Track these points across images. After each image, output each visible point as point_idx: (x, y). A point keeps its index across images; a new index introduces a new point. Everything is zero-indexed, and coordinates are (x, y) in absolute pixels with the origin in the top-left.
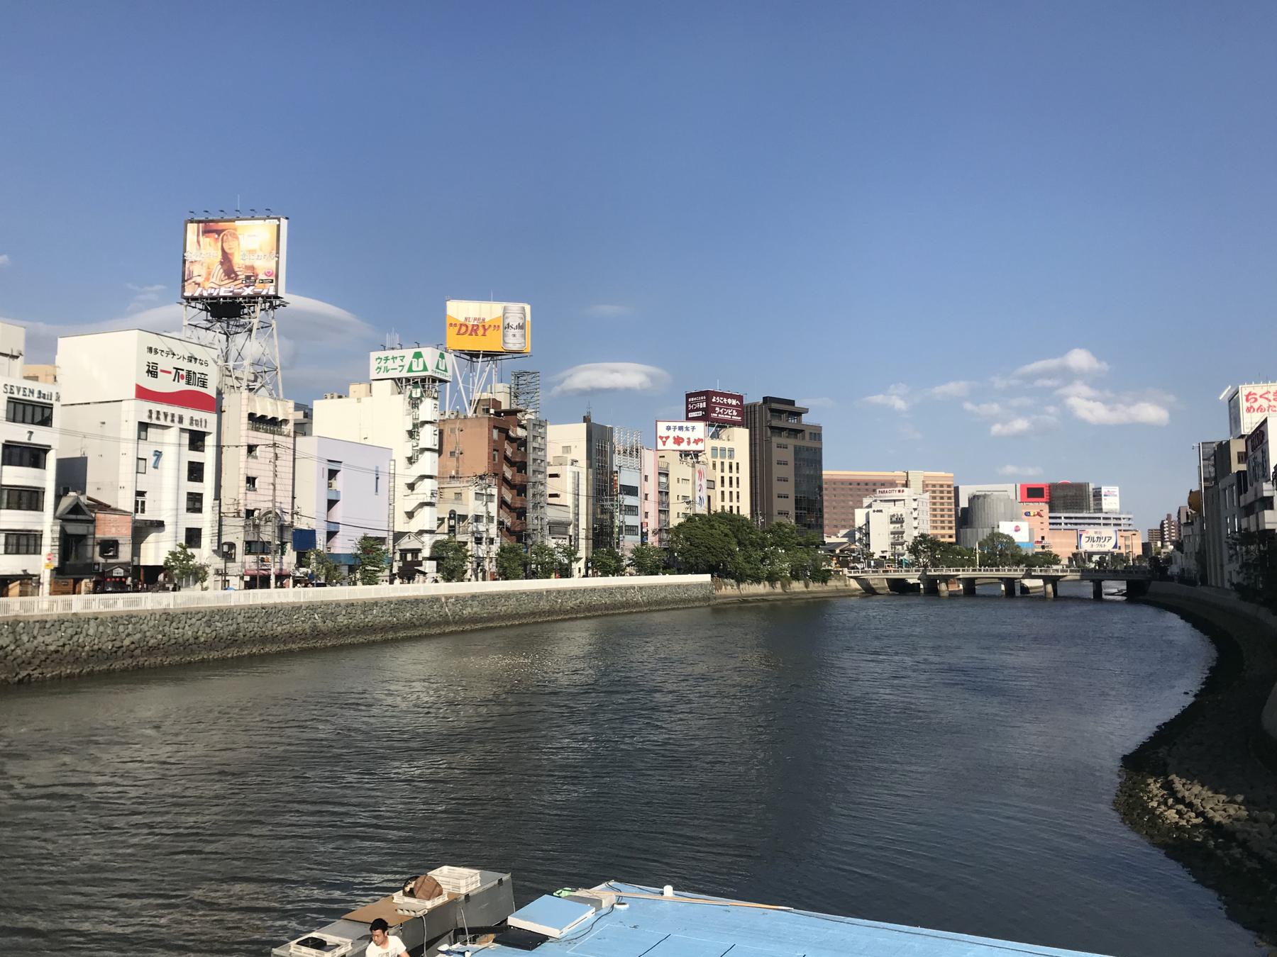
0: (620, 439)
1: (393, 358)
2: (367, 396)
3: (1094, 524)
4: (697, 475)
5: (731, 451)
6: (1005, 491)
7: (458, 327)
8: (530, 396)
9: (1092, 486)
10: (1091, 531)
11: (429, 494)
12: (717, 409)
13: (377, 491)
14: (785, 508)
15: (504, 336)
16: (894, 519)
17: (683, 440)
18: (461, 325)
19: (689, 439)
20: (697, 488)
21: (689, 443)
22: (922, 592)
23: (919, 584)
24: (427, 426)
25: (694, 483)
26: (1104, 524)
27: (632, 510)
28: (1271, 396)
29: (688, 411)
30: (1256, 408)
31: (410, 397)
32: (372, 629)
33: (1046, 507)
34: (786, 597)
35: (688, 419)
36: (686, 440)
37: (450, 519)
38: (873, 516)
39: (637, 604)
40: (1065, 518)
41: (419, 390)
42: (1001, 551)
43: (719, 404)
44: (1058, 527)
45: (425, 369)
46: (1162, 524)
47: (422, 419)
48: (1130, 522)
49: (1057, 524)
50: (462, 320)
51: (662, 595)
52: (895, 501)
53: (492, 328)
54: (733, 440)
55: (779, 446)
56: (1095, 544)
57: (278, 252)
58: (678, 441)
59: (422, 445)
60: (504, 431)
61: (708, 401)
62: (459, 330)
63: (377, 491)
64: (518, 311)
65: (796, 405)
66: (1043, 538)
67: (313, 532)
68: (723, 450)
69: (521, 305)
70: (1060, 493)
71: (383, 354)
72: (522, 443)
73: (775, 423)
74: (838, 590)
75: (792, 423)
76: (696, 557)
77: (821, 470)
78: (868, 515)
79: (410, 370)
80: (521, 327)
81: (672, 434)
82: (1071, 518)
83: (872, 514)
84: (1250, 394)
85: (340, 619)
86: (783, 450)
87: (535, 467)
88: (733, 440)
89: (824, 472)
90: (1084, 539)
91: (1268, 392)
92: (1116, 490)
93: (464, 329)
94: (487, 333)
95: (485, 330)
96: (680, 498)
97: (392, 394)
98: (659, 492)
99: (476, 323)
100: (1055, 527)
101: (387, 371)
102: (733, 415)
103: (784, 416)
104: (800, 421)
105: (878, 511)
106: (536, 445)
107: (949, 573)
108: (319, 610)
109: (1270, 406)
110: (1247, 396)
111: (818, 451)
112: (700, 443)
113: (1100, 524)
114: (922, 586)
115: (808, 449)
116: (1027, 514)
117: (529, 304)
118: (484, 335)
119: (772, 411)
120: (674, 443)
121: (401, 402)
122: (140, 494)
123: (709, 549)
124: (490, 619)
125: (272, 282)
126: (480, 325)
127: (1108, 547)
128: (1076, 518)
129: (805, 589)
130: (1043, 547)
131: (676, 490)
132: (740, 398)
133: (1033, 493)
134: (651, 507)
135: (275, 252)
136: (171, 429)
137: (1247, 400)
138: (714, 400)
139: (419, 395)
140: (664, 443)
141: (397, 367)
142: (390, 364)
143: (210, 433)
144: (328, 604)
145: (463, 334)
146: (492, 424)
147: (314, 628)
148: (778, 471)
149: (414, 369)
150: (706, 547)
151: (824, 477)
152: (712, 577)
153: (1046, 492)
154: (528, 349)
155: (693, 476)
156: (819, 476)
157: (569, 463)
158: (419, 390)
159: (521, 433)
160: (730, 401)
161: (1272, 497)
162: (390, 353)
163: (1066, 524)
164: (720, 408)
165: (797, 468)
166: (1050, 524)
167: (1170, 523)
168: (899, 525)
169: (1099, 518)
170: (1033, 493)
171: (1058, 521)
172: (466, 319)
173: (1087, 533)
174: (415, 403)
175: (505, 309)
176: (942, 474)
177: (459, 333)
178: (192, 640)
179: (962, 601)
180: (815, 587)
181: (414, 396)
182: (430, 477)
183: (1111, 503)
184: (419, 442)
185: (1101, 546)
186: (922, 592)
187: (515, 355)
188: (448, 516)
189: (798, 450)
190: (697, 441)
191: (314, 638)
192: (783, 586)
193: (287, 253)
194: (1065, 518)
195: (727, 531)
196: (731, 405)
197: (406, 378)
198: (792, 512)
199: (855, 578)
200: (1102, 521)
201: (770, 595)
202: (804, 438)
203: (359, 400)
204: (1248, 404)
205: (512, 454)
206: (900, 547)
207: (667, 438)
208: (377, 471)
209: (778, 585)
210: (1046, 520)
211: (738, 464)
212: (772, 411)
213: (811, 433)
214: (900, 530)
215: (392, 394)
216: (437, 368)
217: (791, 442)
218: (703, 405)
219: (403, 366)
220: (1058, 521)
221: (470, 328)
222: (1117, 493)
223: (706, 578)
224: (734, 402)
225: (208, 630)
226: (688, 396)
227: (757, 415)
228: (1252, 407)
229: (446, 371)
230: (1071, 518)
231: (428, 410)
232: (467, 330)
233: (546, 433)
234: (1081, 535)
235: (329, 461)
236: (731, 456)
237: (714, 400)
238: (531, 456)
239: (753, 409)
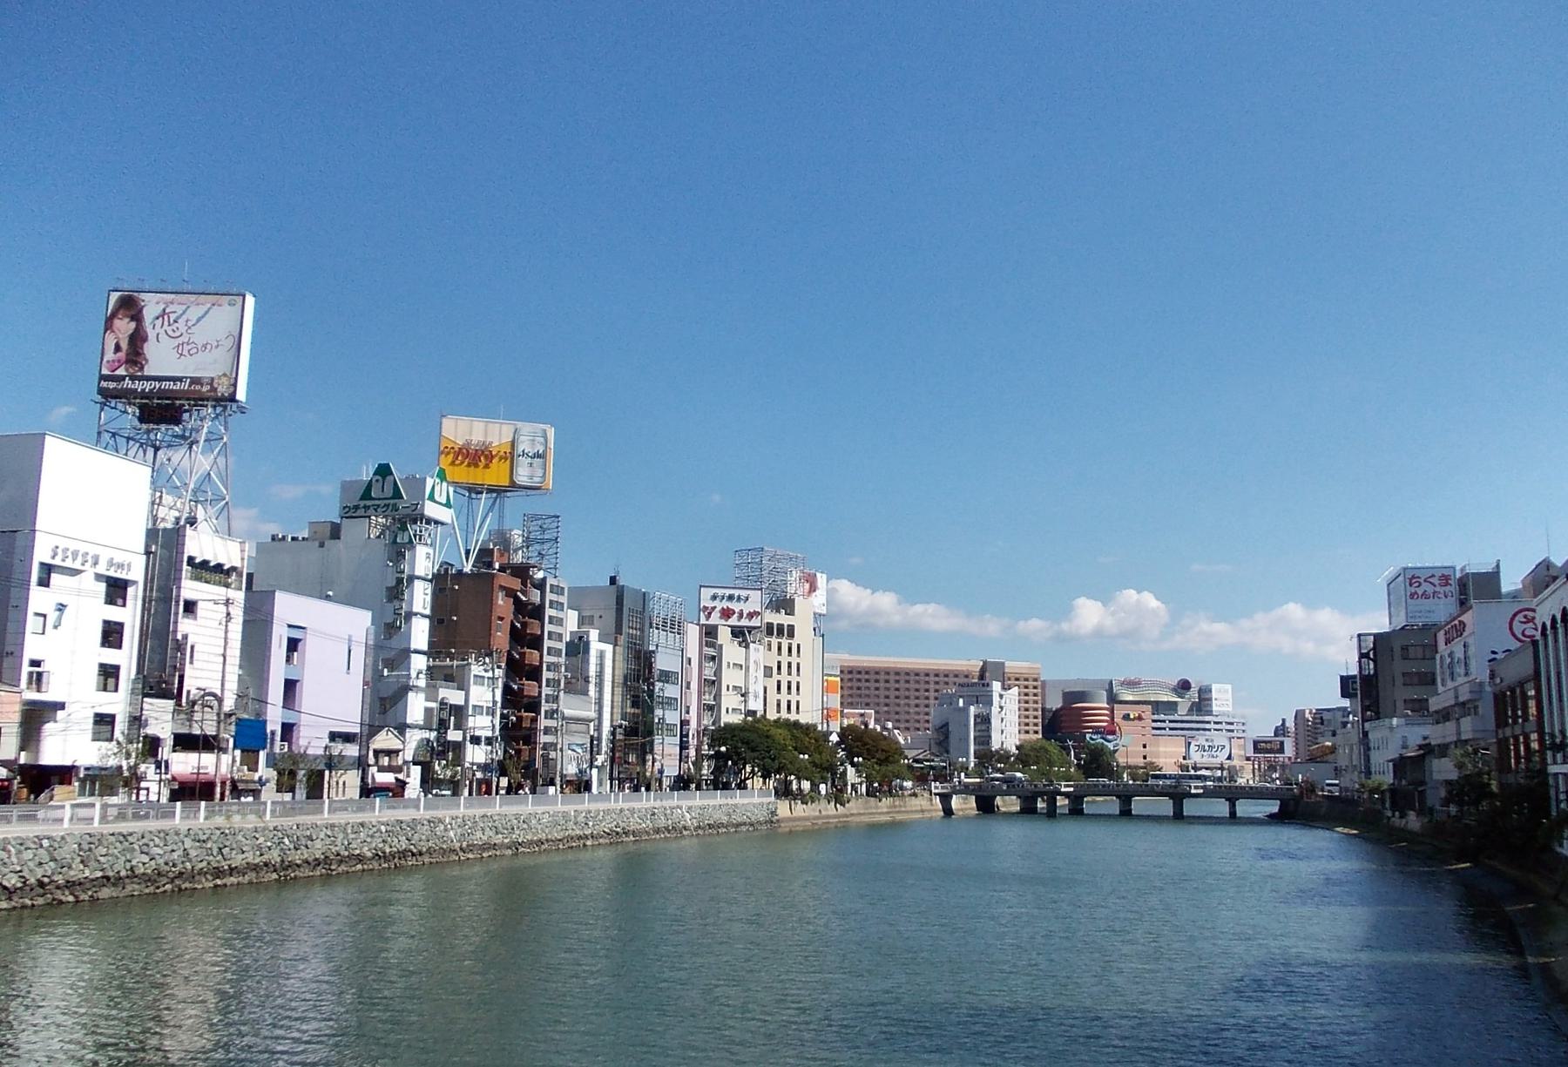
5: (791, 629)
21: (739, 596)
28: (1437, 582)
30: (1420, 594)
56: (1205, 753)
81: (720, 605)
84: (1413, 577)
91: (1433, 576)
96: (731, 688)
100: (1158, 732)
109: (1434, 593)
122: (12, 653)
136: (83, 574)
143: (134, 583)
169: (1209, 722)
173: (1197, 740)
185: (1213, 757)
187: (529, 492)
190: (751, 615)
193: (251, 358)
208: (350, 640)
210: (1148, 722)
211: (799, 646)
225: (145, 859)
228: (1416, 593)
234: (1190, 743)
235: (290, 626)
236: (791, 634)
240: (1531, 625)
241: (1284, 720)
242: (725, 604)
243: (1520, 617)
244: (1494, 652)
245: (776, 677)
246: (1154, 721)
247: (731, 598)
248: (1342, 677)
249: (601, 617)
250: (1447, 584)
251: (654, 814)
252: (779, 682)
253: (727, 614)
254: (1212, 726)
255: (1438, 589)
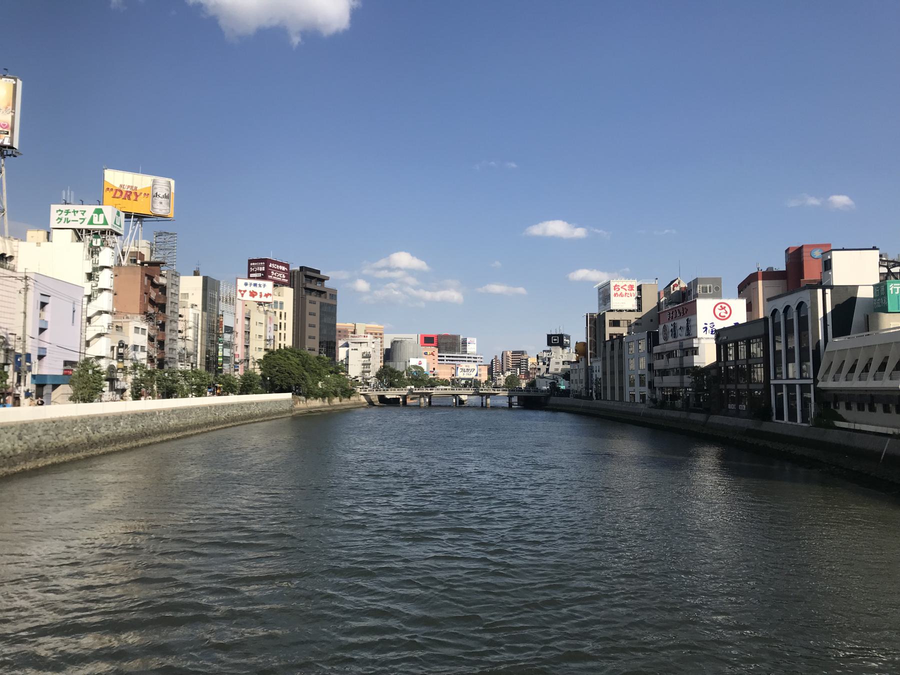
0: (224, 290)
1: (74, 212)
2: (44, 241)
3: (462, 361)
4: (268, 319)
5: (282, 303)
6: (412, 338)
7: (114, 191)
8: (168, 252)
9: (461, 337)
10: (464, 365)
11: (106, 327)
12: (272, 272)
13: (73, 322)
14: (312, 344)
15: (153, 202)
16: (365, 355)
17: (256, 293)
18: (117, 190)
19: (261, 293)
20: (268, 330)
22: (401, 404)
23: (399, 398)
24: (106, 270)
25: (266, 326)
26: (468, 361)
27: (228, 345)
28: (626, 288)
29: (249, 273)
31: (91, 245)
32: (120, 439)
33: (437, 350)
34: (330, 409)
35: (249, 278)
36: (259, 294)
37: (119, 347)
38: (351, 353)
39: (256, 416)
40: (447, 357)
41: (99, 240)
42: (419, 378)
43: (274, 269)
44: (442, 362)
45: (106, 223)
46: (492, 362)
47: (101, 264)
48: (481, 360)
49: (441, 360)
50: (118, 186)
51: (269, 408)
52: (361, 343)
53: (142, 195)
54: (283, 296)
55: (311, 302)
56: (465, 373)
57: (14, 108)
58: (253, 294)
59: (101, 286)
60: (151, 278)
61: (266, 266)
62: (115, 193)
63: (73, 322)
64: (164, 184)
65: (321, 274)
66: (434, 369)
67: (781, 351)
68: (276, 302)
69: (167, 179)
70: (443, 341)
71: (64, 207)
72: (163, 289)
73: (309, 286)
74: (355, 404)
75: (318, 286)
76: (282, 380)
77: (336, 323)
78: (348, 352)
79: (91, 222)
80: (167, 197)
82: (450, 357)
83: (350, 351)
84: (616, 286)
85: (102, 430)
86: (313, 305)
87: (172, 309)
88: (283, 296)
89: (337, 324)
90: (459, 370)
91: (625, 285)
92: (475, 340)
93: (118, 194)
94: (138, 198)
95: (137, 196)
97: (72, 241)
98: (245, 332)
99: (129, 190)
101: (68, 222)
102: (282, 277)
103: (313, 281)
104: (323, 285)
105: (355, 349)
106: (173, 291)
107: (427, 391)
108: (89, 423)
109: (626, 294)
110: (615, 287)
111: (334, 307)
112: (269, 296)
113: (465, 361)
114: (401, 400)
115: (329, 305)
116: (426, 354)
117: (173, 179)
118: (136, 200)
119: (306, 276)
120: (250, 295)
121: (81, 249)
123: (290, 374)
124: (185, 429)
125: (7, 133)
126: (133, 192)
127: (472, 375)
128: (452, 357)
129: (339, 403)
130: (434, 375)
131: (255, 330)
132: (287, 266)
133: (428, 340)
134: (239, 341)
135: (10, 107)
137: (615, 289)
138: (270, 266)
139: (99, 244)
140: (242, 295)
141: (78, 219)
142: (71, 216)
144: (93, 418)
145: (118, 198)
146: (144, 272)
147: (89, 439)
148: (309, 320)
149: (94, 222)
150: (288, 373)
151: (337, 327)
152: (293, 394)
153: (435, 339)
154: (171, 214)
155: (266, 321)
156: (335, 325)
157: (189, 306)
158: (99, 240)
159: (162, 281)
160: (281, 267)
161: (698, 348)
162: (71, 208)
163: (447, 360)
164: (275, 272)
165: (321, 318)
166: (439, 360)
167: (496, 361)
168: (367, 359)
169: (465, 357)
170: (428, 340)
171: (448, 358)
172: (121, 186)
174: (94, 251)
175: (154, 181)
176: (377, 326)
177: (114, 197)
178: (12, 453)
179: (507, 412)
180: (345, 401)
181: (94, 244)
182: (106, 312)
183: (472, 348)
184: (98, 283)
186: (401, 404)
187: (159, 219)
188: (117, 345)
189: (322, 305)
190: (267, 295)
191: (91, 447)
192: (329, 401)
194: (447, 357)
195: (298, 362)
196: (282, 271)
197: (86, 230)
198: (317, 348)
199: (363, 395)
200: (467, 359)
201: (321, 408)
202: (326, 298)
203: (38, 244)
204: (616, 292)
205: (156, 297)
206: (367, 374)
207: (245, 291)
209: (326, 400)
211: (285, 313)
212: (306, 276)
213: (330, 294)
214: (368, 362)
215: (72, 241)
216: (115, 223)
217: (318, 300)
218: (263, 269)
219: (84, 219)
220: (448, 358)
221: (124, 193)
222: (475, 342)
223: (289, 395)
224: (284, 268)
225: (21, 443)
226: (250, 261)
227: (296, 279)
229: (120, 226)
230: (450, 357)
231: (106, 257)
232: (121, 195)
233: (179, 282)
235: (42, 294)
236: (281, 308)
237: (270, 266)
238: (170, 300)
239: (292, 275)
240: (724, 311)
241: (496, 356)
242: (253, 288)
243: (719, 307)
244: (706, 324)
245: (279, 331)
246: (439, 356)
247: (255, 285)
248: (548, 335)
249: (193, 294)
250: (632, 290)
251: (242, 408)
252: (280, 334)
253: (253, 294)
254: (467, 359)
255: (628, 292)
